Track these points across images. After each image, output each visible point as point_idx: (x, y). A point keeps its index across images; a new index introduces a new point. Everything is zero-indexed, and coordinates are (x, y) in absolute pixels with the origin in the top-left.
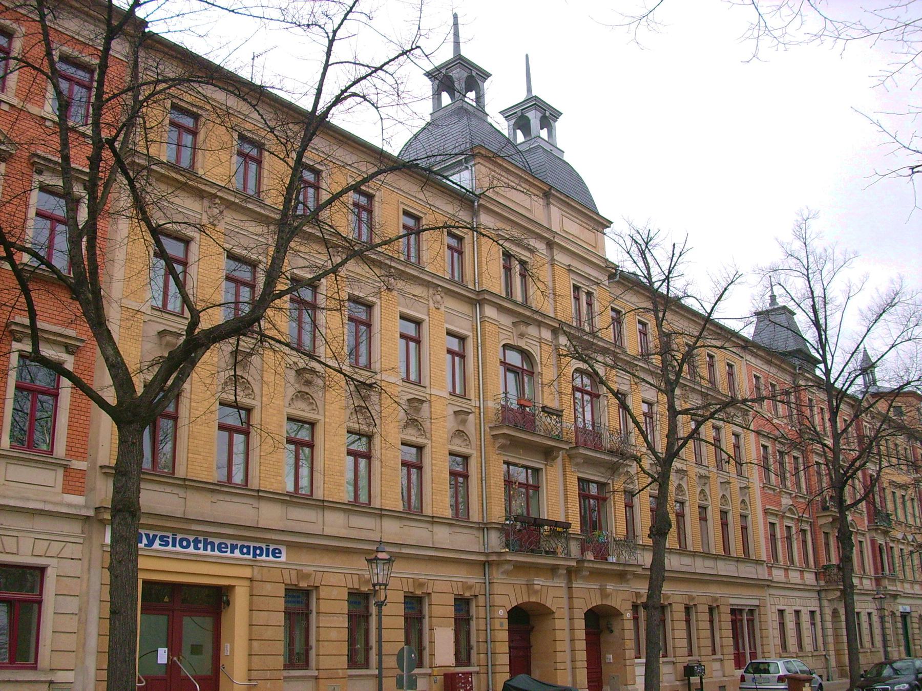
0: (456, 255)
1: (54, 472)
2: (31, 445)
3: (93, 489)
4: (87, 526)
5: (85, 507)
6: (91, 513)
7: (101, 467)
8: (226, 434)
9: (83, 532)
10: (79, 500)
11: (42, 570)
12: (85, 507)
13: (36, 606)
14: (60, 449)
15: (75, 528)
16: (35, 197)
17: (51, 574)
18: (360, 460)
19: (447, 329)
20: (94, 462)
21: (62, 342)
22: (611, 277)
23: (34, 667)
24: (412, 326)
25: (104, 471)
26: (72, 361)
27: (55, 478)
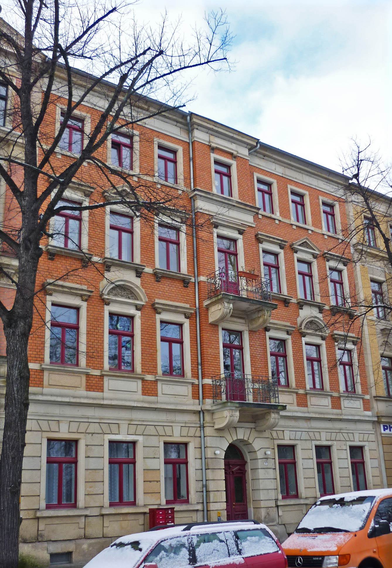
0: (330, 217)
1: (292, 396)
2: (63, 361)
3: (373, 408)
4: (374, 425)
5: (372, 416)
6: (376, 419)
7: (374, 397)
8: (167, 344)
9: (373, 429)
10: (369, 413)
11: (76, 441)
12: (372, 416)
13: (183, 466)
14: (138, 368)
15: (369, 426)
16: (108, 220)
17: (367, 449)
18: (174, 345)
19: (371, 278)
20: (371, 395)
21: (182, 311)
22: (251, 148)
23: (75, 506)
24: (272, 257)
25: (376, 398)
26: (140, 315)
27: (136, 386)
